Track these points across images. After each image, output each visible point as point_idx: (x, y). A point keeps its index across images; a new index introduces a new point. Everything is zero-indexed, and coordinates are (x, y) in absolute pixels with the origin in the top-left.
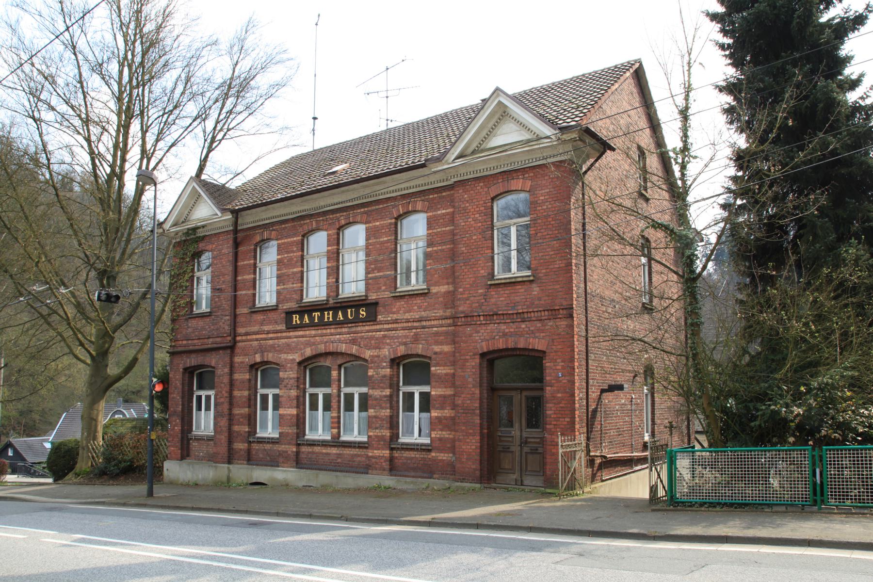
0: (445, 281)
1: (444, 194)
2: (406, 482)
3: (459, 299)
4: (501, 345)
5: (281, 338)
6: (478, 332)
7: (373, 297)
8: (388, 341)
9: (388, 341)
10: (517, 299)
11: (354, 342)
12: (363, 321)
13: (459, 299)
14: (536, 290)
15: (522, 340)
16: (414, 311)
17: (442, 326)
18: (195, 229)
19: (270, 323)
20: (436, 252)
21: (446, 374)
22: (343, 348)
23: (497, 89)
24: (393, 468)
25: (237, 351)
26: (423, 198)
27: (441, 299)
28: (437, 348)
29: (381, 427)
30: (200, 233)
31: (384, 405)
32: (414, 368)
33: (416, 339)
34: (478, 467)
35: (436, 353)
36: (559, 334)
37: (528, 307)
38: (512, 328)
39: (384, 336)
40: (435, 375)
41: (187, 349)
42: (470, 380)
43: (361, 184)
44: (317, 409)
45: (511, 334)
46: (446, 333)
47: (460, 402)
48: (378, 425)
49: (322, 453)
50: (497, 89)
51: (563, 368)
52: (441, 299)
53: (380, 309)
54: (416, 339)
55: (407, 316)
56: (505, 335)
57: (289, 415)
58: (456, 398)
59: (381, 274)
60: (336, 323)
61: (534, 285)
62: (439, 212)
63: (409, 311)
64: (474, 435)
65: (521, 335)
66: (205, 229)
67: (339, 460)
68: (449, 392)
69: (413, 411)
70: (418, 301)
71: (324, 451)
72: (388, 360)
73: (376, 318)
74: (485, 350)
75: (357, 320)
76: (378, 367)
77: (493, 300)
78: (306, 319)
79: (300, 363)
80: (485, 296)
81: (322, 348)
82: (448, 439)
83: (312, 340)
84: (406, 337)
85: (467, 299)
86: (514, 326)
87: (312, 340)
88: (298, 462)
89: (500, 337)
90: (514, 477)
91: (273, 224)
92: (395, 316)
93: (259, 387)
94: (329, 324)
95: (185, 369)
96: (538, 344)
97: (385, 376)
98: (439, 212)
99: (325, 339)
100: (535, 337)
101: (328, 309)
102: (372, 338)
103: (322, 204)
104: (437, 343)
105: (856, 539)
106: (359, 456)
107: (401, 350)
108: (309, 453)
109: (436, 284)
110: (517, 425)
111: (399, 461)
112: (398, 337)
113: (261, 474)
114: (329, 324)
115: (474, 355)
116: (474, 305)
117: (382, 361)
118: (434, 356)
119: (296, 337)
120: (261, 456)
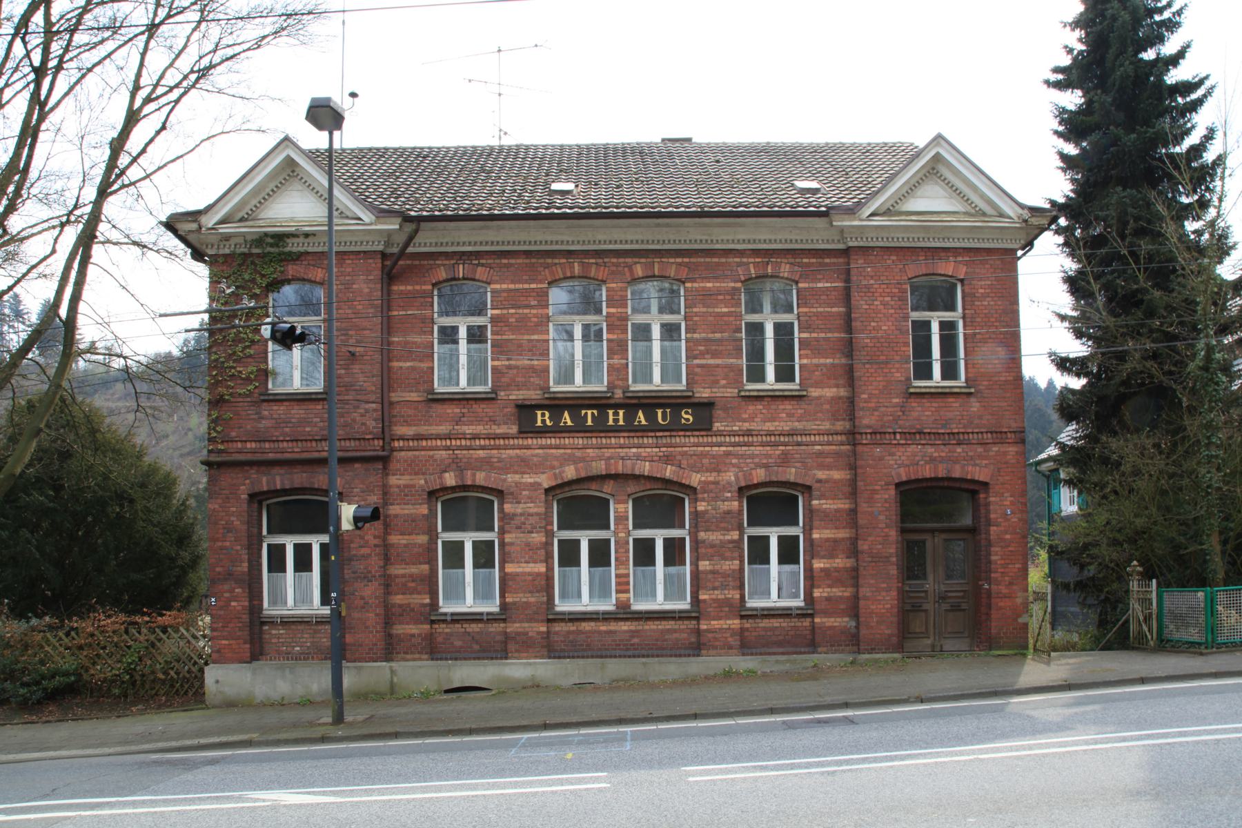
0: (833, 382)
1: (827, 260)
2: (777, 662)
3: (863, 409)
4: (927, 472)
5: (506, 448)
6: (892, 454)
7: (703, 393)
8: (734, 461)
9: (734, 461)
10: (949, 415)
11: (668, 459)
12: (686, 428)
13: (863, 409)
14: (975, 406)
15: (958, 467)
16: (781, 420)
17: (829, 444)
18: (280, 238)
19: (479, 421)
20: (817, 340)
21: (837, 511)
22: (646, 468)
23: (939, 139)
24: (746, 645)
25: (393, 466)
26: (792, 260)
27: (827, 407)
28: (821, 474)
29: (724, 587)
30: (294, 246)
31: (728, 554)
32: (771, 502)
33: (785, 460)
34: (896, 631)
35: (819, 481)
36: (1006, 463)
37: (964, 427)
38: (943, 452)
39: (728, 454)
40: (818, 510)
41: (259, 457)
42: (882, 517)
43: (697, 220)
44: (577, 563)
45: (942, 460)
46: (837, 454)
47: (866, 547)
48: (717, 584)
49: (600, 632)
50: (939, 139)
51: (1012, 503)
52: (827, 407)
53: (718, 413)
54: (785, 460)
55: (769, 426)
56: (932, 459)
57: (530, 574)
58: (860, 542)
59: (719, 361)
60: (631, 428)
61: (973, 399)
62: (820, 285)
63: (773, 420)
64: (888, 590)
65: (956, 461)
66: (310, 239)
67: (636, 640)
68: (843, 534)
69: (767, 561)
70: (788, 406)
71: (603, 628)
72: (735, 488)
73: (711, 423)
74: (904, 479)
75: (675, 427)
76: (716, 499)
77: (915, 414)
78: (567, 418)
79: (547, 491)
80: (902, 408)
81: (599, 467)
82: (841, 598)
83: (578, 453)
84: (767, 456)
85: (875, 409)
86: (946, 449)
87: (578, 453)
88: (552, 650)
89: (926, 463)
90: (929, 642)
91: (478, 255)
92: (746, 426)
93: (440, 529)
94: (616, 430)
95: (252, 496)
96: (981, 476)
97: (729, 512)
98: (820, 285)
99: (608, 453)
100: (975, 465)
101: (616, 407)
102: (704, 455)
103: (600, 237)
104: (822, 467)
105: (1160, 674)
106: (675, 631)
107: (760, 475)
108: (569, 632)
109: (817, 385)
110: (931, 577)
111: (795, 635)
112: (752, 456)
113: (466, 672)
114: (616, 430)
115: (887, 484)
116: (885, 419)
117: (724, 489)
118: (816, 486)
119: (542, 447)
120: (458, 643)
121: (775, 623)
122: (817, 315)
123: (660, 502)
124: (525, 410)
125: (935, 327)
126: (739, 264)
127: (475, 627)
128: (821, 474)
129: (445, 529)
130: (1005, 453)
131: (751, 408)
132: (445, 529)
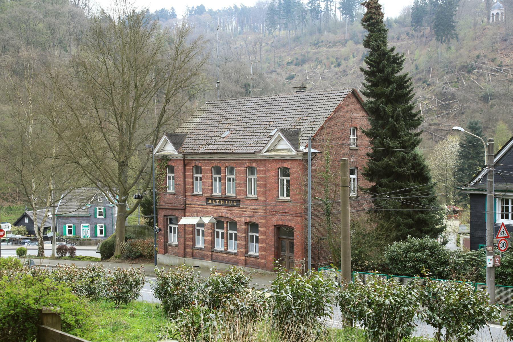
14: (291, 205)
22: (228, 216)
25: (187, 211)
28: (260, 221)
33: (253, 216)
39: (243, 213)
46: (263, 216)
53: (241, 203)
54: (253, 216)
55: (250, 207)
70: (254, 202)
92: (246, 206)
102: (238, 213)
109: (260, 196)
121: (253, 259)
122: (260, 177)
123: (233, 225)
124: (207, 199)
125: (232, 192)
126: (245, 163)
127: (200, 251)
128: (260, 221)
129: (250, 232)
130: (297, 219)
131: (248, 202)
132: (250, 232)
